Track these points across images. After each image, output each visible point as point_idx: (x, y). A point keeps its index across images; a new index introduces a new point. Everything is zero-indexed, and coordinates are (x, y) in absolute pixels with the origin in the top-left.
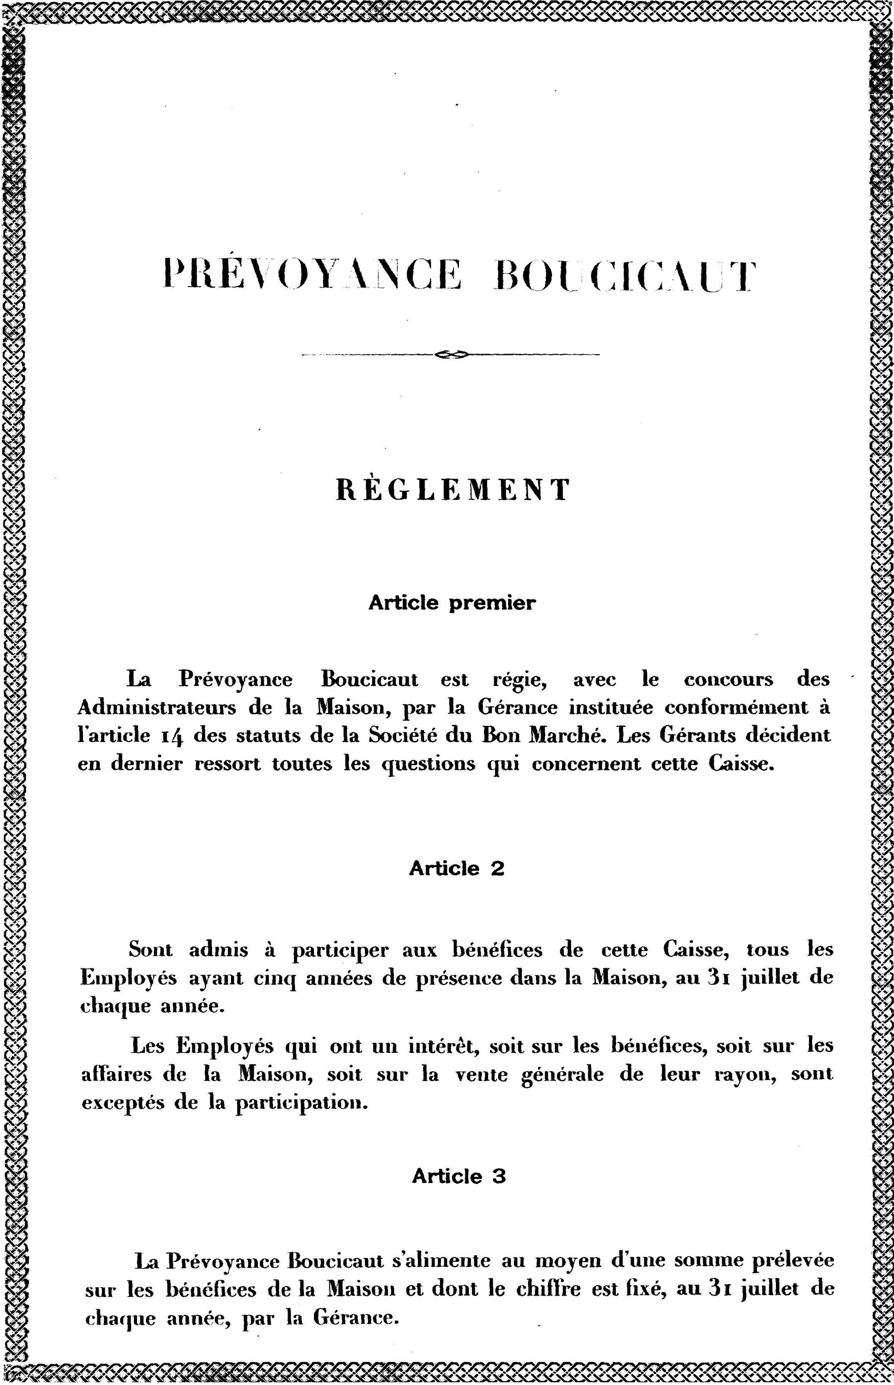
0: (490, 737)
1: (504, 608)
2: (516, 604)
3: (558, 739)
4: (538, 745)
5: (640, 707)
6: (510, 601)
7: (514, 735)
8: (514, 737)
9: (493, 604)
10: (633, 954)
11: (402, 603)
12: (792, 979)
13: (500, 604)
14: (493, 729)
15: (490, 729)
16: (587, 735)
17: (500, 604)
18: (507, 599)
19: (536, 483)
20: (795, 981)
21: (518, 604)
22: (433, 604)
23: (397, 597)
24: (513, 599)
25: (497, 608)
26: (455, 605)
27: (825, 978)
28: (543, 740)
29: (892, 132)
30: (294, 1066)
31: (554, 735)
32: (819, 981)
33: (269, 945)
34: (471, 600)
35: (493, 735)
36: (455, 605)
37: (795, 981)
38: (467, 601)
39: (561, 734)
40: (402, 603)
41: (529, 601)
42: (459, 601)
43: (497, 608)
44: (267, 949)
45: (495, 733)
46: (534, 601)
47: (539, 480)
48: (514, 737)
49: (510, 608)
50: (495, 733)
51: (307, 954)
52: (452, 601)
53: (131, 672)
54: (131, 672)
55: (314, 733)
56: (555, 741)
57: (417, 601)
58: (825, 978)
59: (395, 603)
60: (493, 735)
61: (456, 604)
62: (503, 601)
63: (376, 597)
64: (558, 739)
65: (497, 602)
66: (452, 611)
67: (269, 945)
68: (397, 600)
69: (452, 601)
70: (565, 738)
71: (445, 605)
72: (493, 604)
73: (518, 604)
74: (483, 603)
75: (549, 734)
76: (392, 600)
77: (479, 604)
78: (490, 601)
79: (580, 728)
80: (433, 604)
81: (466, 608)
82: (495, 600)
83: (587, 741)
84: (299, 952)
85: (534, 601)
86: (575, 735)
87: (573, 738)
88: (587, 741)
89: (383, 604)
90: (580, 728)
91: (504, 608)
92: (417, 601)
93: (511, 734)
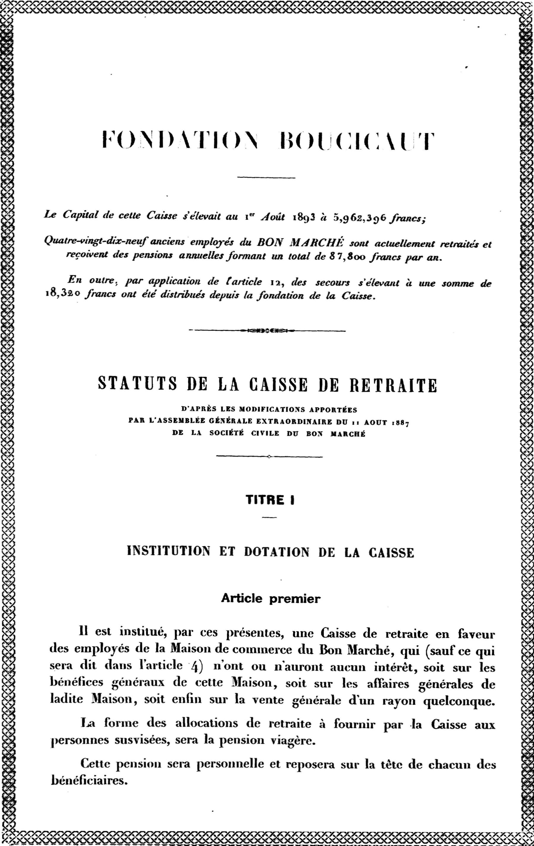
0: (324, 651)
1: (302, 602)
2: (309, 599)
3: (364, 652)
4: (352, 656)
5: (154, 739)
6: (305, 598)
7: (338, 650)
8: (338, 651)
9: (295, 600)
10: (101, 766)
11: (241, 599)
12: (276, 765)
13: (300, 599)
14: (326, 646)
15: (324, 647)
16: (382, 650)
17: (300, 599)
18: (303, 596)
19: (307, 550)
20: (278, 766)
21: (310, 600)
22: (259, 599)
23: (238, 595)
24: (307, 597)
25: (298, 602)
26: (273, 600)
27: (418, 765)
28: (355, 653)
29: (533, 350)
30: (118, 776)
31: (362, 650)
32: (414, 767)
33: (322, 722)
34: (283, 597)
35: (326, 650)
36: (273, 600)
37: (278, 766)
38: (280, 598)
39: (366, 650)
40: (241, 599)
41: (317, 598)
42: (276, 598)
43: (298, 602)
44: (321, 724)
45: (327, 649)
46: (319, 598)
47: (308, 548)
48: (338, 651)
49: (305, 602)
50: (327, 649)
51: (392, 727)
52: (271, 598)
53: (83, 719)
54: (83, 719)
55: (175, 681)
56: (362, 653)
57: (250, 597)
58: (418, 765)
59: (237, 598)
60: (326, 650)
61: (274, 600)
62: (301, 597)
63: (226, 595)
64: (364, 652)
65: (297, 598)
66: (271, 604)
67: (322, 722)
68: (238, 596)
69: (271, 598)
70: (368, 652)
71: (266, 600)
72: (295, 600)
73: (310, 600)
74: (290, 599)
75: (359, 650)
76: (235, 597)
77: (287, 599)
78: (293, 598)
79: (377, 646)
80: (259, 599)
81: (280, 602)
82: (296, 597)
83: (381, 654)
84: (388, 726)
85: (319, 598)
86: (374, 650)
87: (373, 652)
88: (381, 654)
89: (230, 599)
90: (377, 646)
91: (302, 602)
92: (250, 597)
93: (336, 649)
